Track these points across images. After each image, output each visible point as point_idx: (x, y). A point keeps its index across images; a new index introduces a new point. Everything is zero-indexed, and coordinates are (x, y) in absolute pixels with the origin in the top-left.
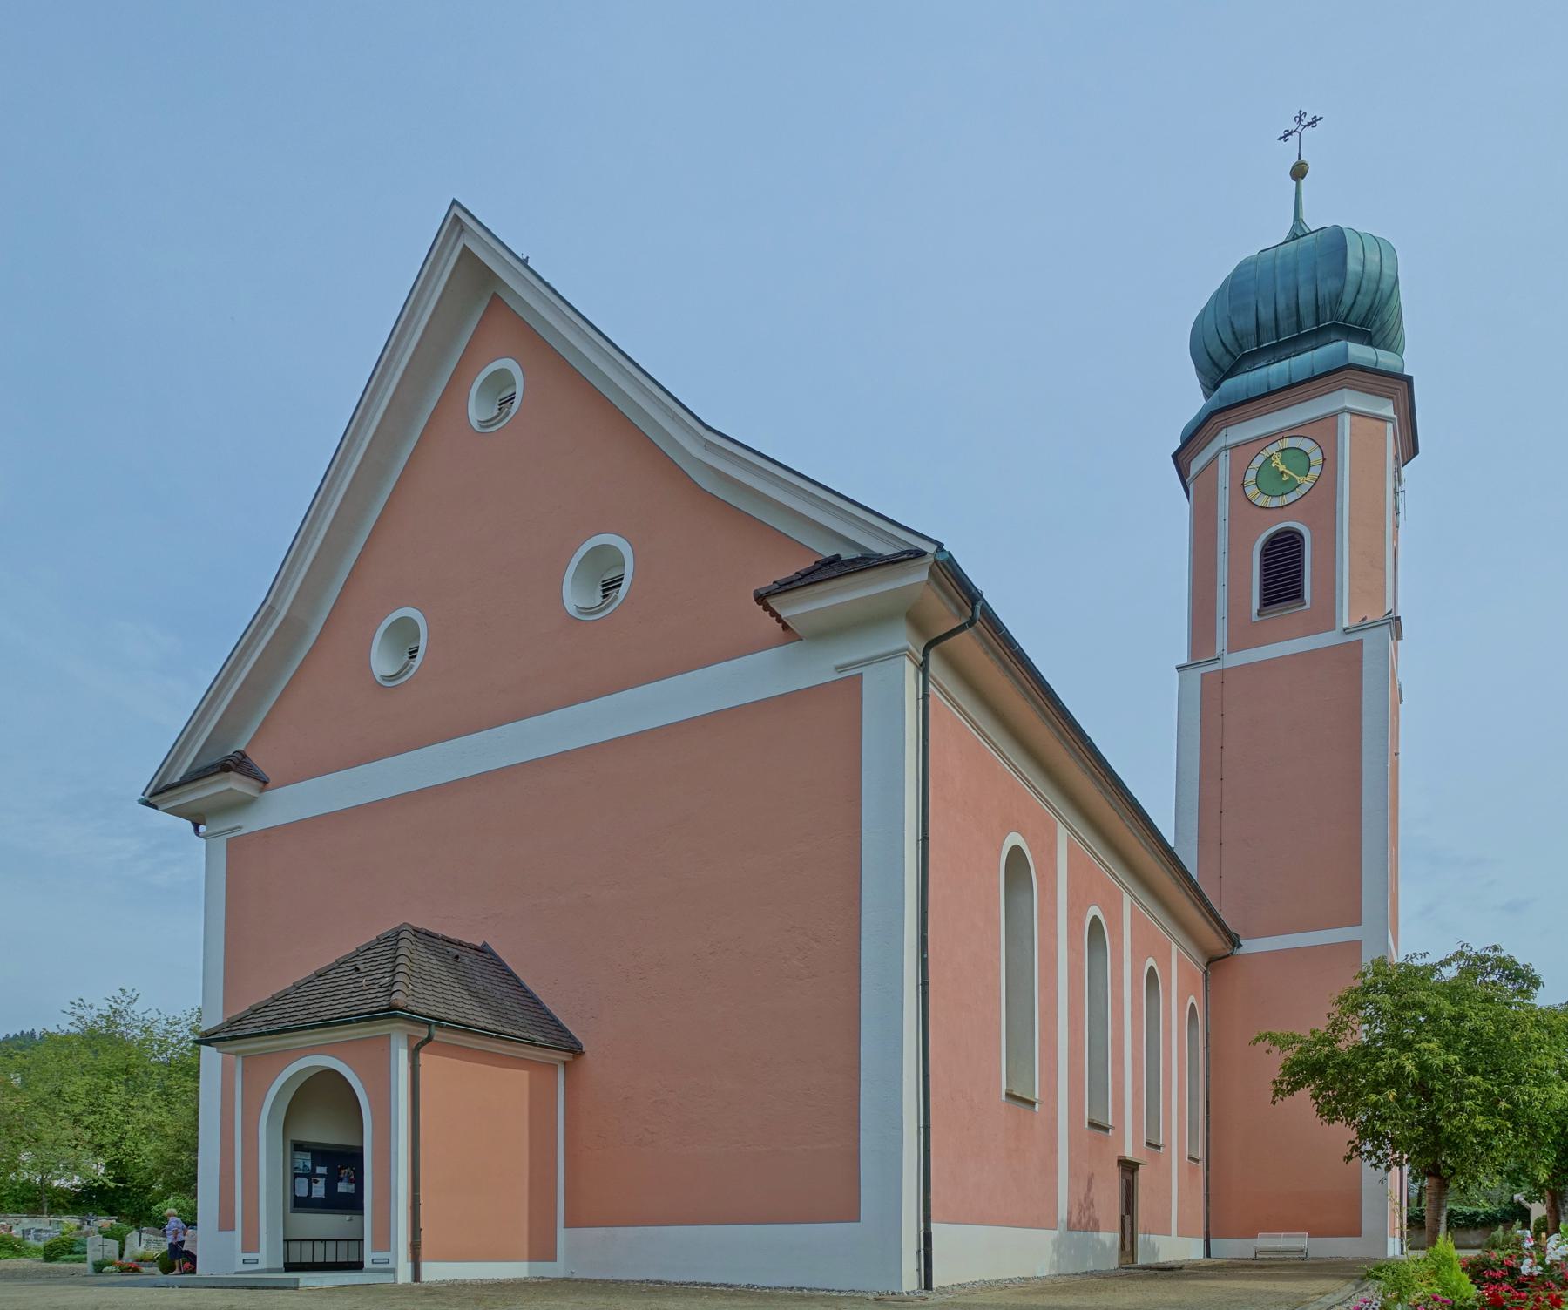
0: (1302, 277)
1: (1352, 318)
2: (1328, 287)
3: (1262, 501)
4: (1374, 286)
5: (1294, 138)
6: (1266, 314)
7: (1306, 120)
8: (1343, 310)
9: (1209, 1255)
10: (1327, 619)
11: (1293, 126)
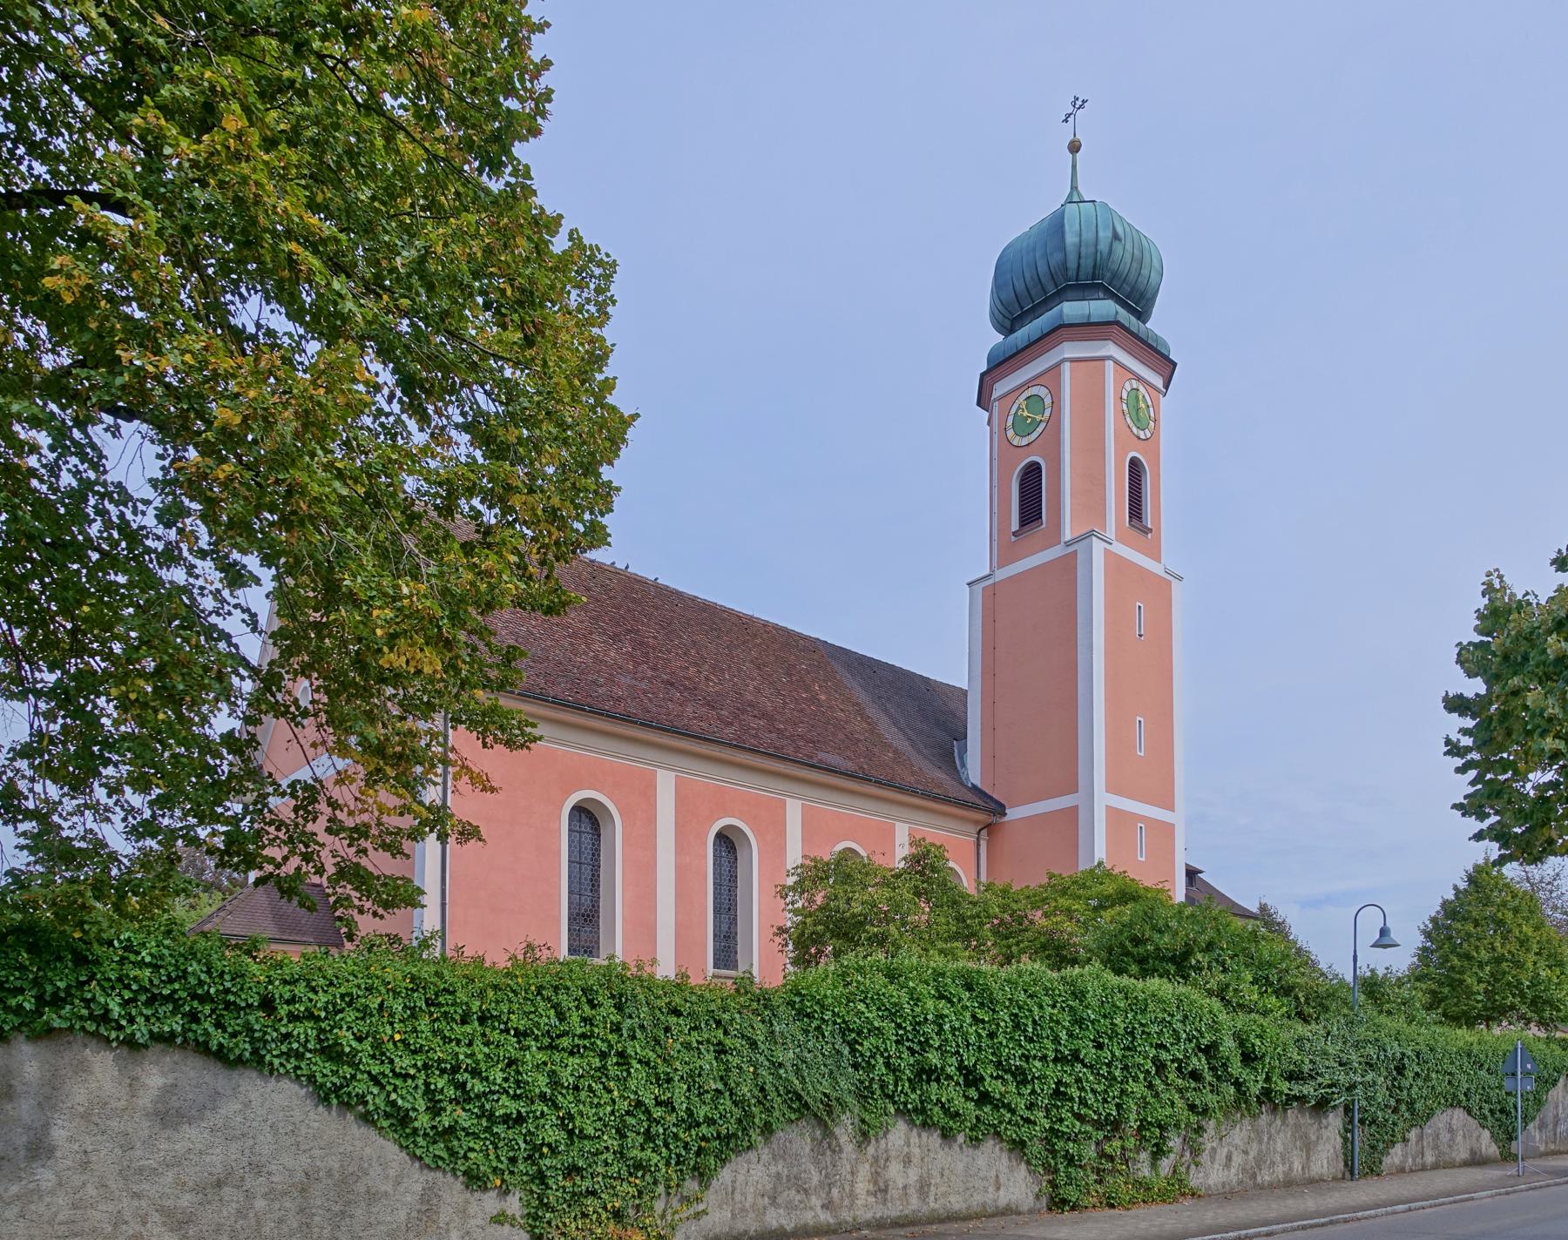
0: (1038, 254)
1: (1082, 276)
2: (1056, 258)
3: (1025, 442)
4: (1092, 250)
5: (1071, 119)
6: (1020, 286)
7: (1079, 103)
8: (1072, 273)
9: (588, 818)
10: (1055, 536)
11: (1071, 109)
